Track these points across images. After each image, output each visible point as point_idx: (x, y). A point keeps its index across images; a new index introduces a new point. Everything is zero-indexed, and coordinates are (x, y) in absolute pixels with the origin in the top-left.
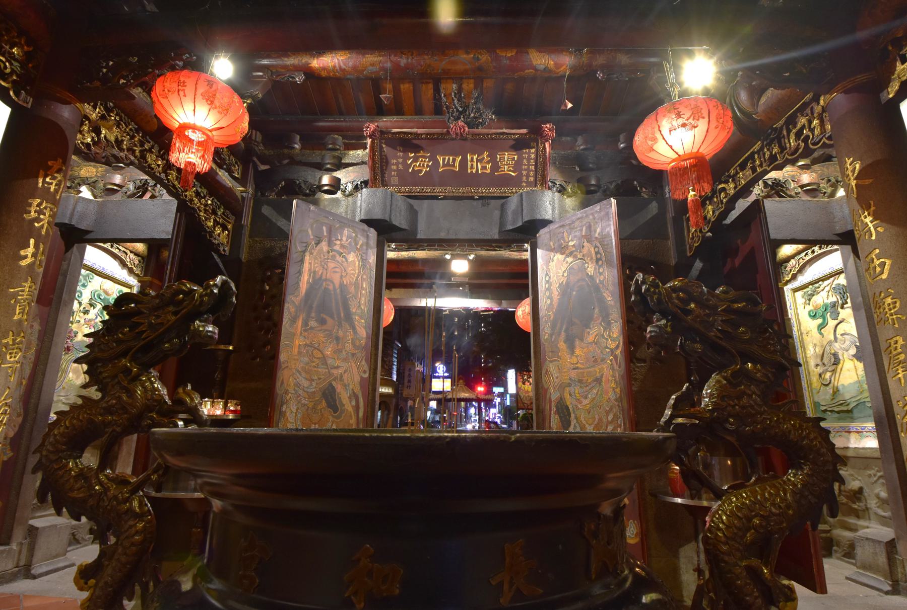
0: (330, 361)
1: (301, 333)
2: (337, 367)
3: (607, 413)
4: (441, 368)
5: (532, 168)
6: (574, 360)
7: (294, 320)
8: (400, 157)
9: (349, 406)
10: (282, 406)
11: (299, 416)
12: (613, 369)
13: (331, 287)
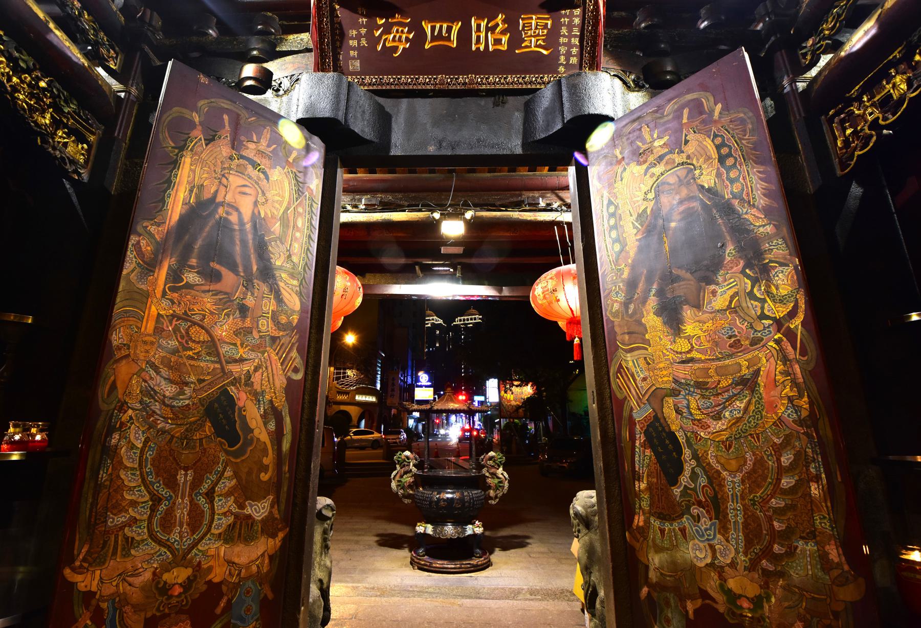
0: (224, 349)
1: (164, 294)
2: (242, 360)
3: (778, 450)
4: (424, 378)
5: (576, 41)
6: (682, 345)
7: (149, 266)
8: (363, 26)
9: (262, 433)
10: (109, 434)
11: (149, 455)
12: (785, 359)
13: (234, 218)
